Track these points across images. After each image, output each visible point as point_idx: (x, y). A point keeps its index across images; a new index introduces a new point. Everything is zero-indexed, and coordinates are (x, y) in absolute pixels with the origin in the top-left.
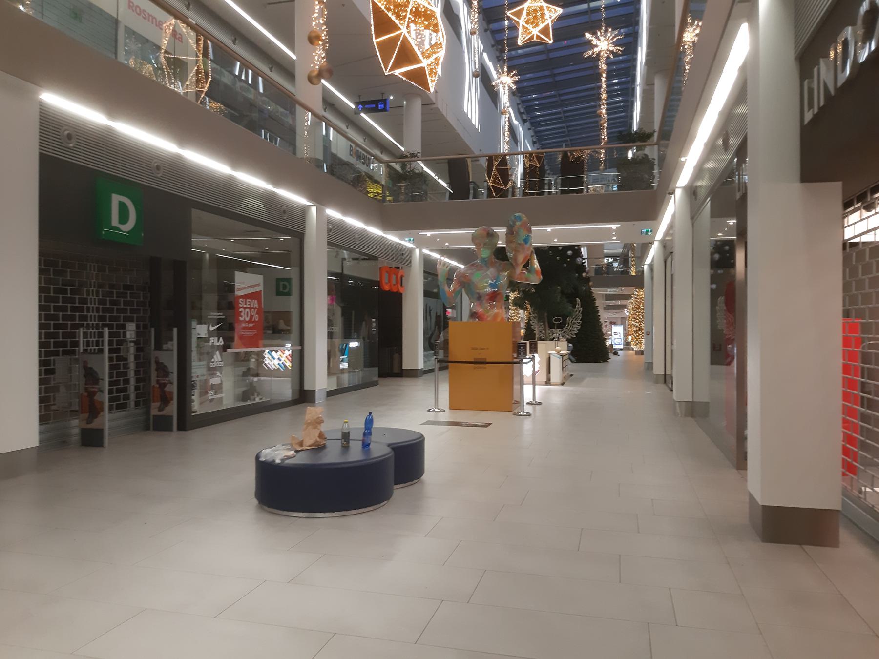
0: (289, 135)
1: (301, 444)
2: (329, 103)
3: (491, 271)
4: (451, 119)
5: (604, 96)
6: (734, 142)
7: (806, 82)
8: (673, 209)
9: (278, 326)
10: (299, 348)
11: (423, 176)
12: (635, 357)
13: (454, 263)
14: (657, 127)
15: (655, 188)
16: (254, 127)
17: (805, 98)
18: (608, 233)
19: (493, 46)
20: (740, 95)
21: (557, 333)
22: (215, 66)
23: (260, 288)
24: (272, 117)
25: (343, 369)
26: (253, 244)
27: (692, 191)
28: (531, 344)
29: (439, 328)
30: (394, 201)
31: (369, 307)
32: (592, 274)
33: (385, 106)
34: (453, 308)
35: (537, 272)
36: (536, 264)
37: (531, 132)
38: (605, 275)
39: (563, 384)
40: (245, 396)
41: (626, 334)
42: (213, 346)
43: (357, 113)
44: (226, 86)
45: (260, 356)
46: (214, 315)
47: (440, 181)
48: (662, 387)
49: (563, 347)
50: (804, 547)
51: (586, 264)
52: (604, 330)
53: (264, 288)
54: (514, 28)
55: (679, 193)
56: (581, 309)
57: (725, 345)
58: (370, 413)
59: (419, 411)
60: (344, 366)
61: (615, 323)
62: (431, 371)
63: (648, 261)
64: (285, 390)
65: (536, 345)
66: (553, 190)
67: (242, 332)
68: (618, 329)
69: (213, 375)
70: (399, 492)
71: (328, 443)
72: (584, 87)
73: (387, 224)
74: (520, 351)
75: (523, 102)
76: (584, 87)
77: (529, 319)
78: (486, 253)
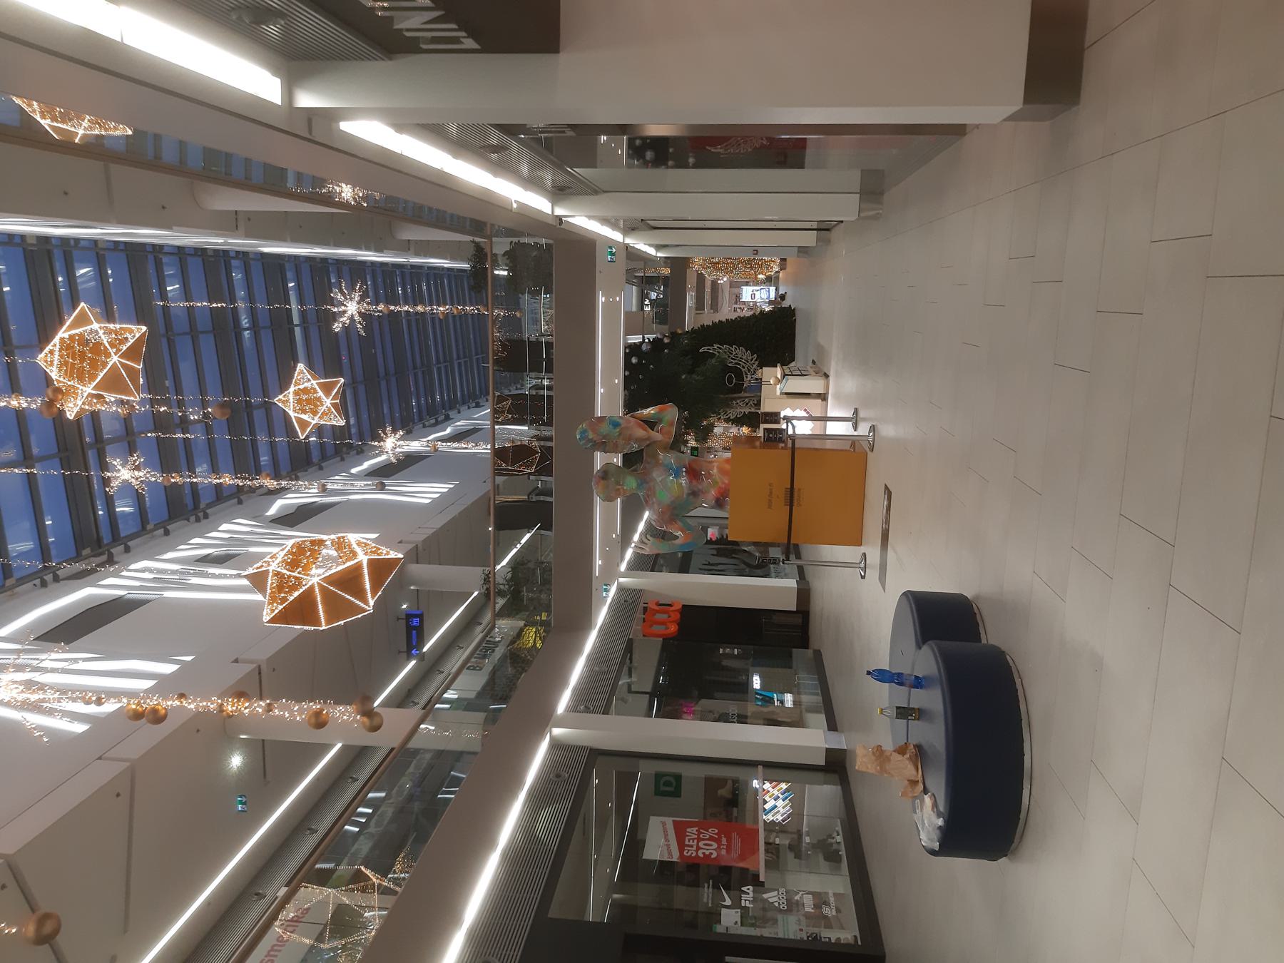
0: (446, 760)
1: (913, 783)
2: (403, 698)
3: (657, 475)
4: (439, 522)
5: (420, 308)
6: (495, 138)
7: (424, 47)
8: (583, 220)
9: (725, 798)
10: (760, 768)
11: (516, 565)
12: (789, 269)
13: (641, 526)
14: (469, 238)
15: (551, 242)
16: (434, 811)
17: (445, 46)
18: (611, 308)
19: (343, 459)
20: (433, 131)
21: (748, 380)
22: (346, 860)
23: (669, 821)
24: (420, 782)
25: (794, 702)
26: (603, 824)
27: (559, 193)
28: (766, 422)
29: (734, 551)
30: (548, 610)
31: (700, 656)
32: (665, 328)
33: (416, 616)
34: (705, 530)
35: (661, 411)
36: (650, 411)
37: (464, 408)
38: (667, 311)
39: (827, 376)
40: (832, 857)
41: (757, 283)
42: (754, 900)
43: (422, 657)
44: (372, 849)
45: (771, 826)
46: (706, 893)
47: (523, 541)
48: (835, 234)
49: (772, 374)
50: (1087, 44)
51: (652, 337)
52: (747, 313)
53: (669, 816)
54: (320, 430)
55: (559, 211)
56: (716, 346)
57: (780, 150)
58: (869, 673)
59: (867, 592)
60: (789, 699)
61: (738, 297)
62: (801, 570)
63: (652, 251)
64: (823, 794)
65: (767, 414)
66: (546, 383)
67: (734, 855)
68: (747, 293)
69: (799, 904)
70: (992, 635)
71: (913, 741)
72: (406, 336)
73: (584, 623)
74: (775, 438)
75: (421, 419)
76: (406, 336)
77: (727, 420)
78: (631, 483)
